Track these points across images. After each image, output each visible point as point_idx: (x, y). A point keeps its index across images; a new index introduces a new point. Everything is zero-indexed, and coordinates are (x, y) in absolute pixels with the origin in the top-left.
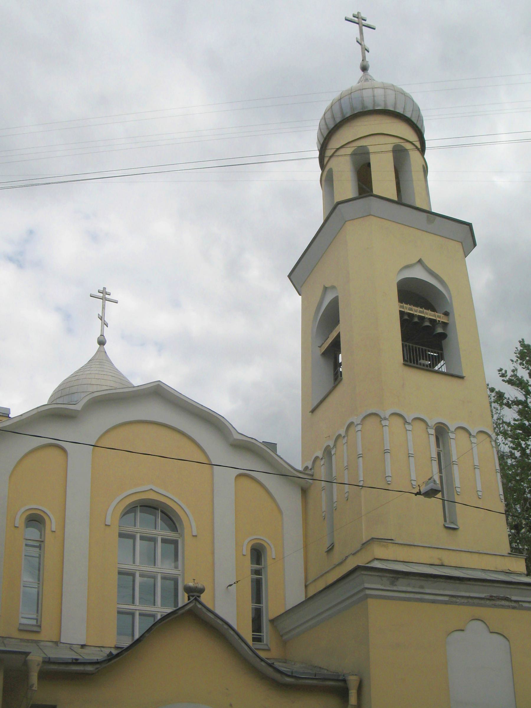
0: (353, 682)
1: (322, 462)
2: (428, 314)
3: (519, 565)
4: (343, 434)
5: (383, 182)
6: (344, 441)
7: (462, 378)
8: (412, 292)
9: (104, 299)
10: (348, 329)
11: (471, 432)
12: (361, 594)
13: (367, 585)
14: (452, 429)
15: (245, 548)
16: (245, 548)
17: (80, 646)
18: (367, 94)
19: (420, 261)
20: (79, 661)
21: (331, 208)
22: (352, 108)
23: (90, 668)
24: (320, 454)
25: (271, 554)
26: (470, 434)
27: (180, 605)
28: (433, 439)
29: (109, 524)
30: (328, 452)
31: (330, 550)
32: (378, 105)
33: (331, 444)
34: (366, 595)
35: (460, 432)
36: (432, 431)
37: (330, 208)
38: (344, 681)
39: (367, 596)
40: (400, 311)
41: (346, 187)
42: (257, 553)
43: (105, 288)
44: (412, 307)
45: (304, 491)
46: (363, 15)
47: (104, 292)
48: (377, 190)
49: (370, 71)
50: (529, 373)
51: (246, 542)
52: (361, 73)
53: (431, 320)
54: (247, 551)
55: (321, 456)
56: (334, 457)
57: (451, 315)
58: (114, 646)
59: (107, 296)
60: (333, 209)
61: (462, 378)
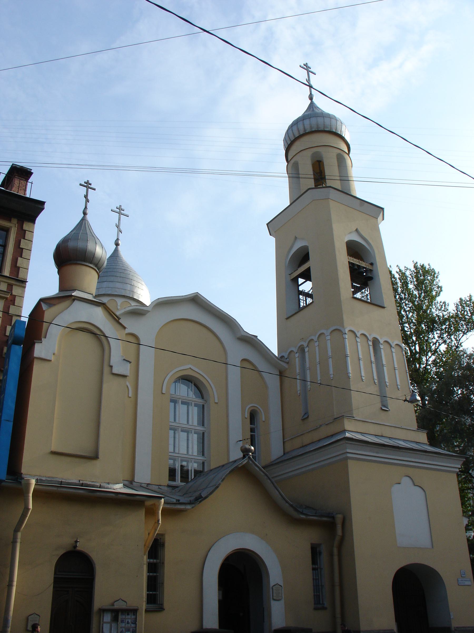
0: (339, 517)
1: (297, 355)
2: (363, 264)
3: (422, 437)
4: (286, 357)
5: (331, 170)
7: (384, 307)
8: (354, 250)
9: (120, 213)
11: (391, 344)
12: (344, 456)
13: (348, 451)
14: (381, 341)
15: (246, 413)
16: (246, 413)
17: (203, 495)
19: (357, 230)
20: (180, 501)
22: (311, 127)
23: (182, 507)
25: (262, 417)
26: (391, 346)
27: (232, 459)
30: (302, 350)
31: (305, 418)
32: (327, 128)
33: (305, 344)
34: (347, 457)
35: (363, 336)
36: (371, 343)
38: (333, 518)
39: (347, 458)
40: (349, 262)
42: (253, 416)
43: (120, 206)
44: (353, 258)
45: (281, 374)
46: (309, 65)
47: (120, 208)
51: (247, 408)
52: (310, 101)
53: (357, 265)
54: (247, 415)
56: (307, 354)
57: (374, 265)
58: (166, 485)
59: (122, 212)
61: (384, 307)
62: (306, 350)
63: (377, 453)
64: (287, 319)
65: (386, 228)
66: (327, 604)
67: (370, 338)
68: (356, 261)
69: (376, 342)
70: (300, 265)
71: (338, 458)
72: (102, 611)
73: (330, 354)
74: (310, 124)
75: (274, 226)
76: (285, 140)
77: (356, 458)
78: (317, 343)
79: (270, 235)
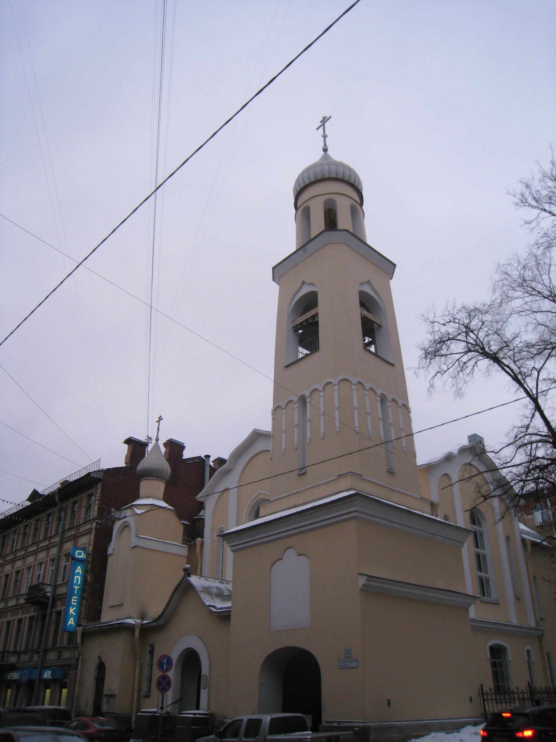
1: (296, 406)
4: (283, 407)
5: (344, 221)
6: (284, 411)
10: (324, 312)
18: (326, 167)
19: (369, 282)
21: (303, 244)
24: (295, 398)
28: (379, 403)
29: (360, 577)
36: (379, 399)
37: (301, 246)
41: (318, 222)
48: (340, 226)
49: (328, 152)
50: (257, 436)
52: (323, 153)
55: (295, 401)
60: (306, 243)
62: (308, 400)
63: (254, 536)
64: (287, 367)
65: (396, 284)
66: (54, 614)
67: (379, 394)
68: (365, 313)
69: (383, 399)
70: (303, 313)
71: (367, 517)
72: (105, 695)
73: (337, 405)
74: (329, 170)
75: (280, 271)
76: (295, 188)
77: (306, 530)
78: (309, 399)
79: (273, 280)
